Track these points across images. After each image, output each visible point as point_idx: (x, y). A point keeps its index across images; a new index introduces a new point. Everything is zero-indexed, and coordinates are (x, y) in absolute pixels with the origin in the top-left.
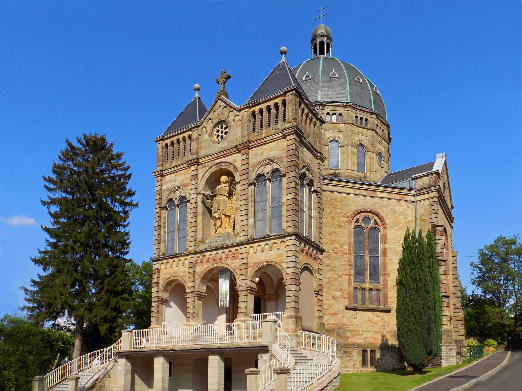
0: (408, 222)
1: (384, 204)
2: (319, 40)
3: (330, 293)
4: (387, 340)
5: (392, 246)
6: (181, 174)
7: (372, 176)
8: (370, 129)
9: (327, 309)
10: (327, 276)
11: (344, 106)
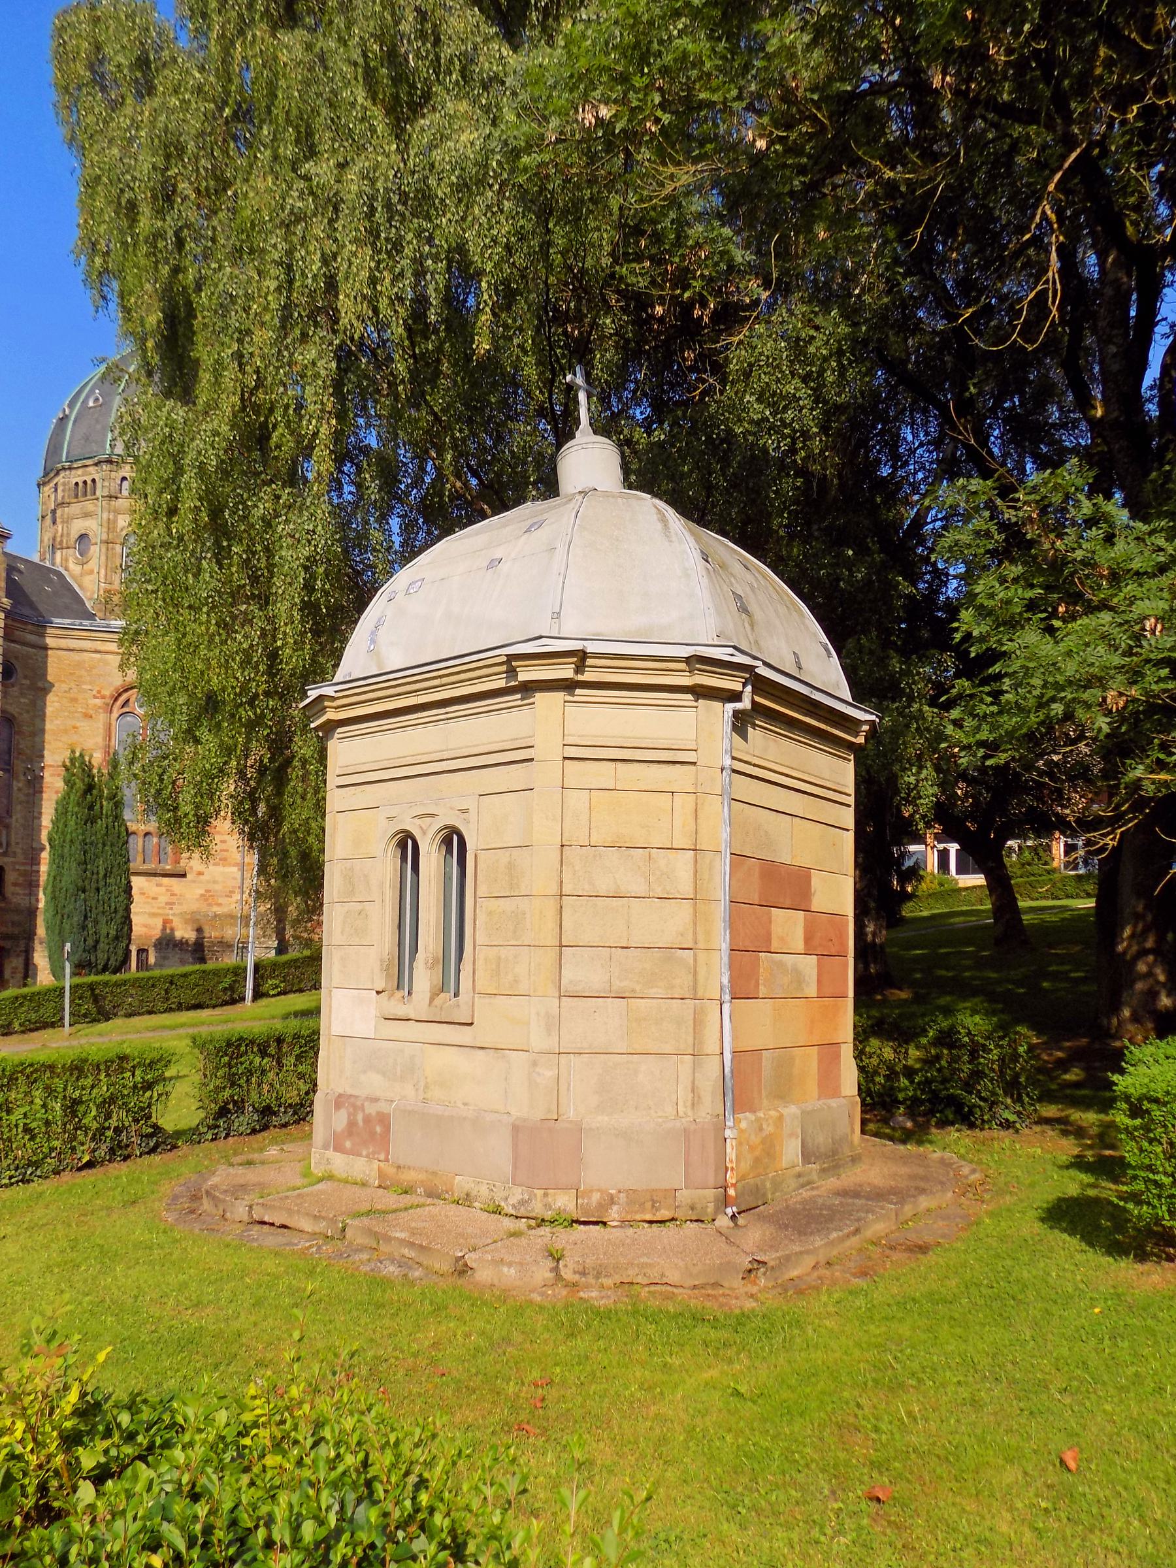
4: (172, 930)
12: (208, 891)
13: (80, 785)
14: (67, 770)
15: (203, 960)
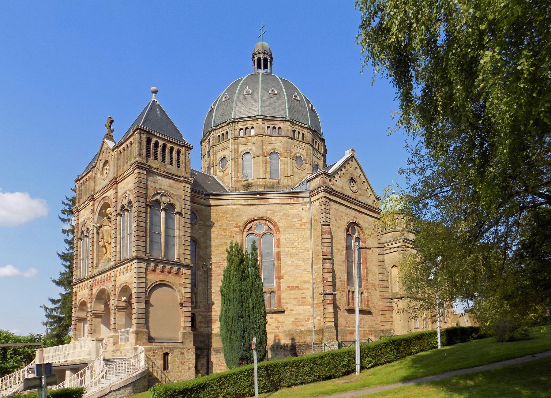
0: (302, 224)
1: (277, 210)
2: (256, 58)
4: (279, 340)
5: (286, 249)
7: (286, 180)
8: (283, 137)
11: (254, 120)
12: (296, 319)
13: (236, 260)
14: (229, 253)
15: (295, 355)
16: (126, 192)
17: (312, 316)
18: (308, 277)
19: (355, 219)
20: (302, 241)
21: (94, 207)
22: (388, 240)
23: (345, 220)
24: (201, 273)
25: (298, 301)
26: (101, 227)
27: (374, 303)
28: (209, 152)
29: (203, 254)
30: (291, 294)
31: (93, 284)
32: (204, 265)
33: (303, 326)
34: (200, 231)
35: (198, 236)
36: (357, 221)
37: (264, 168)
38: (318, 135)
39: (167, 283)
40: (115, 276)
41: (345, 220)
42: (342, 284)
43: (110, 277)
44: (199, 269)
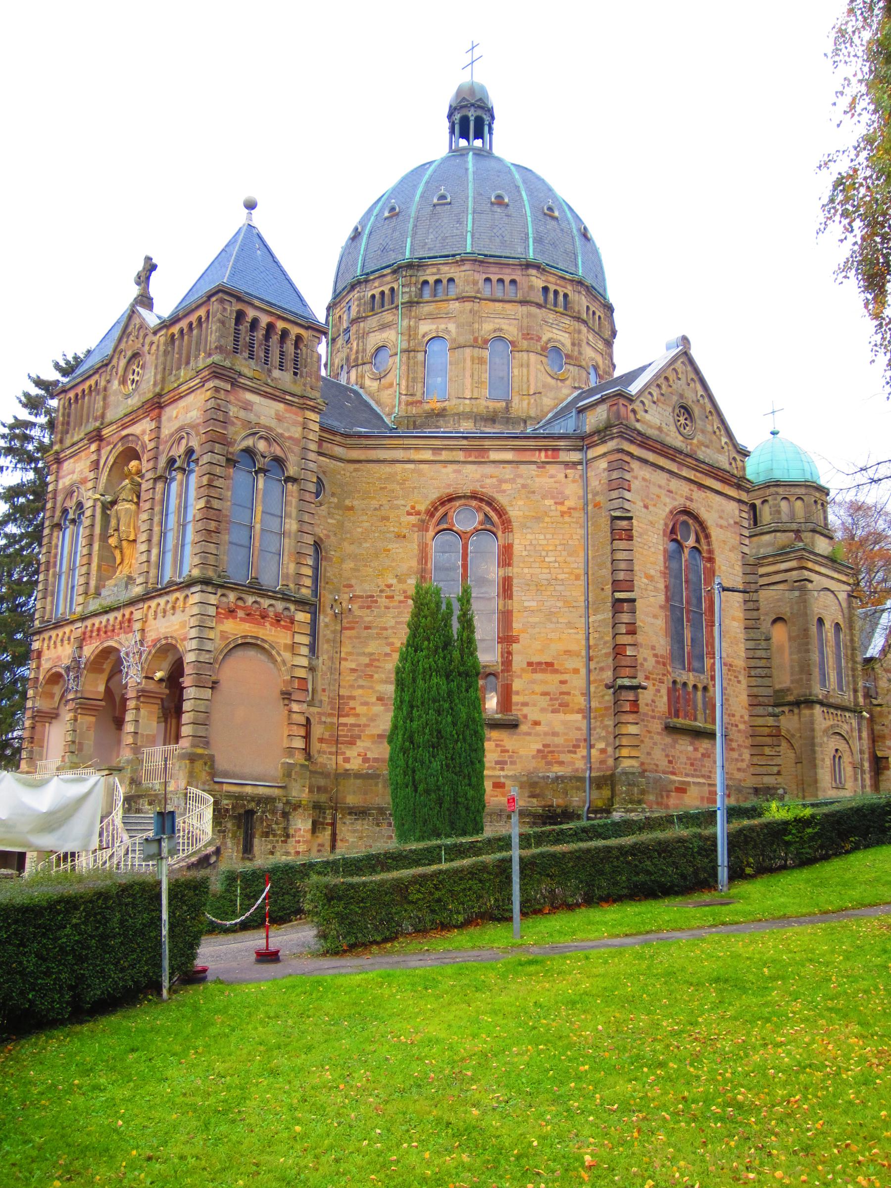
1: (507, 477)
3: (371, 688)
5: (526, 570)
6: (80, 458)
9: (365, 726)
10: (367, 650)
12: (545, 746)
16: (181, 429)
17: (585, 740)
18: (576, 641)
19: (688, 503)
20: (564, 553)
21: (99, 455)
22: (762, 551)
23: (665, 505)
24: (327, 620)
25: (551, 699)
26: (114, 503)
27: (733, 715)
28: (347, 330)
29: (334, 575)
30: (533, 682)
31: (84, 633)
32: (336, 600)
33: (561, 763)
34: (330, 521)
35: (325, 532)
36: (693, 506)
37: (476, 373)
38: (600, 298)
39: (259, 642)
40: (144, 620)
41: (665, 505)
42: (657, 662)
43: (130, 621)
44: (324, 611)
